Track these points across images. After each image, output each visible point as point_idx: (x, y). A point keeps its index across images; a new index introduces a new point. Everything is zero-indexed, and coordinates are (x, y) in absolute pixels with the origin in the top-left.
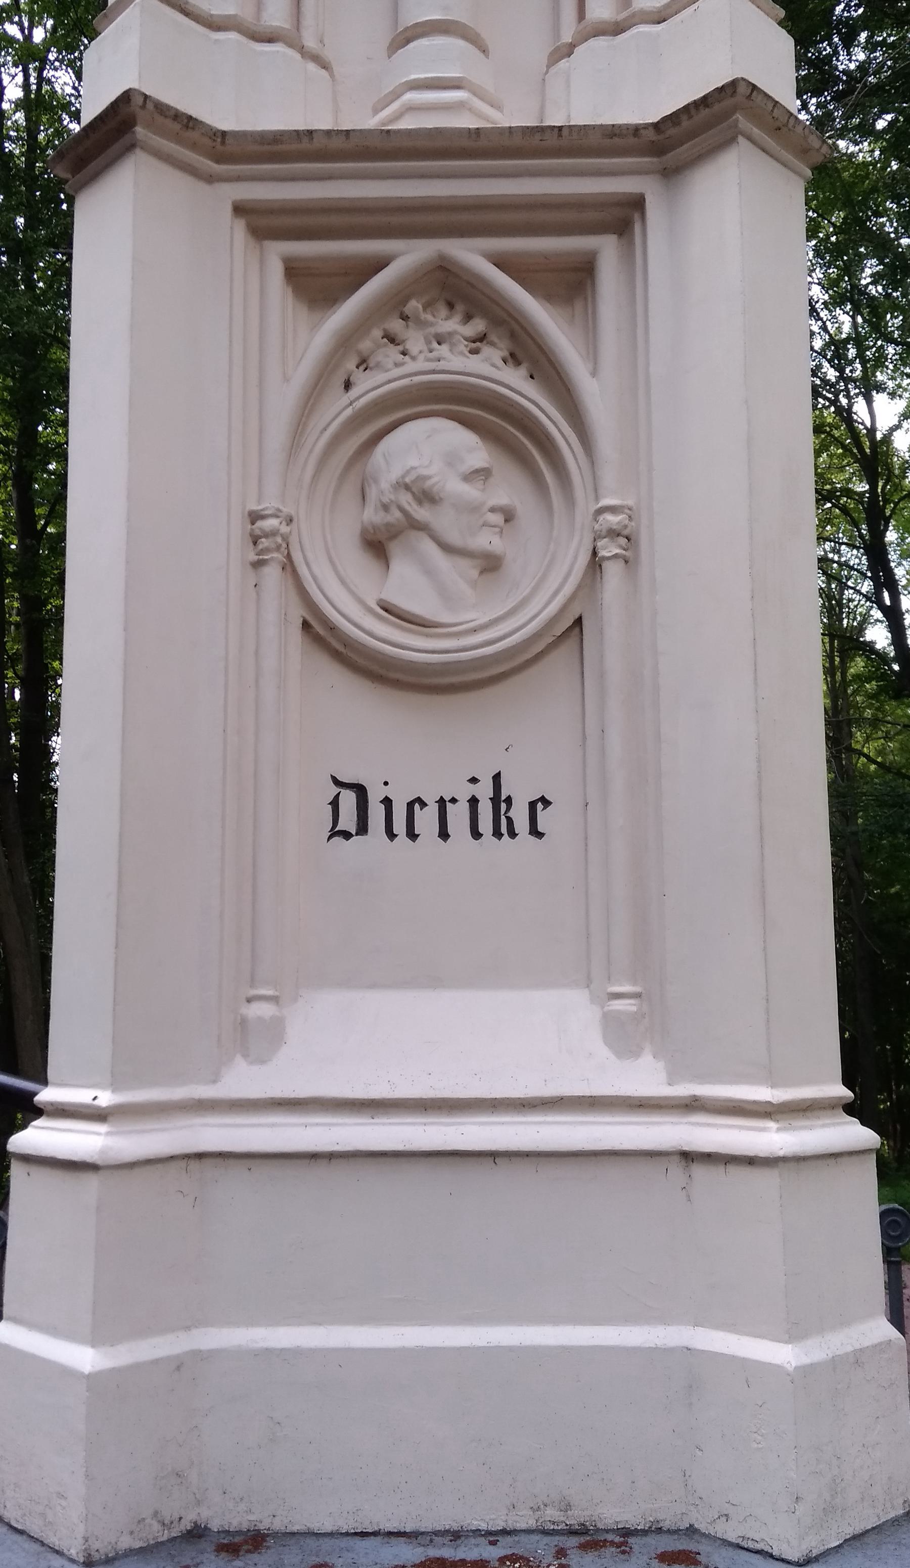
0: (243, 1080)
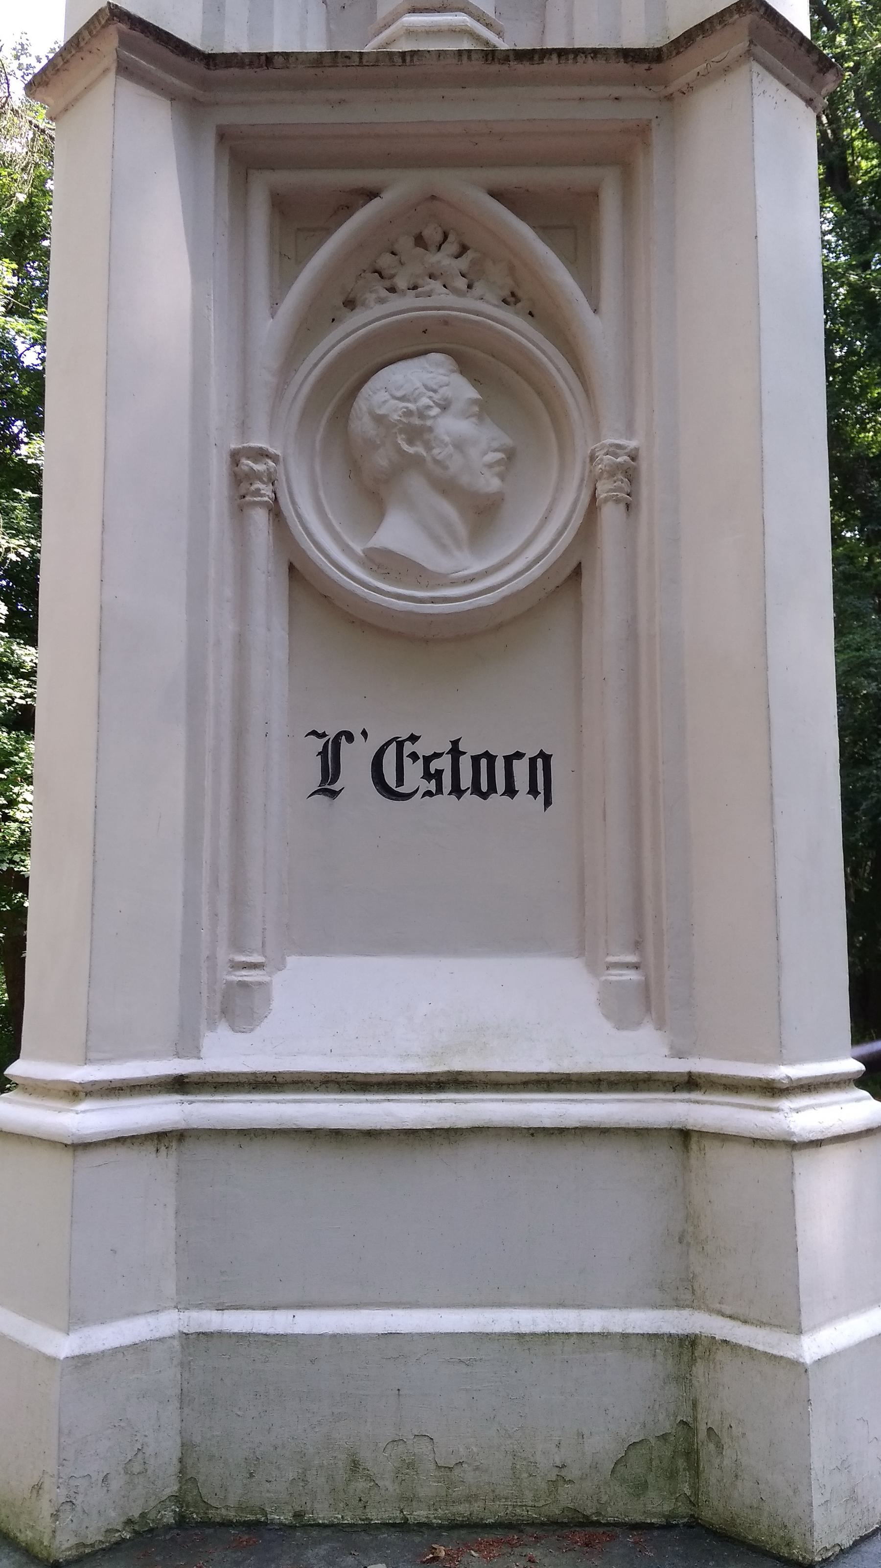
0: (224, 1051)
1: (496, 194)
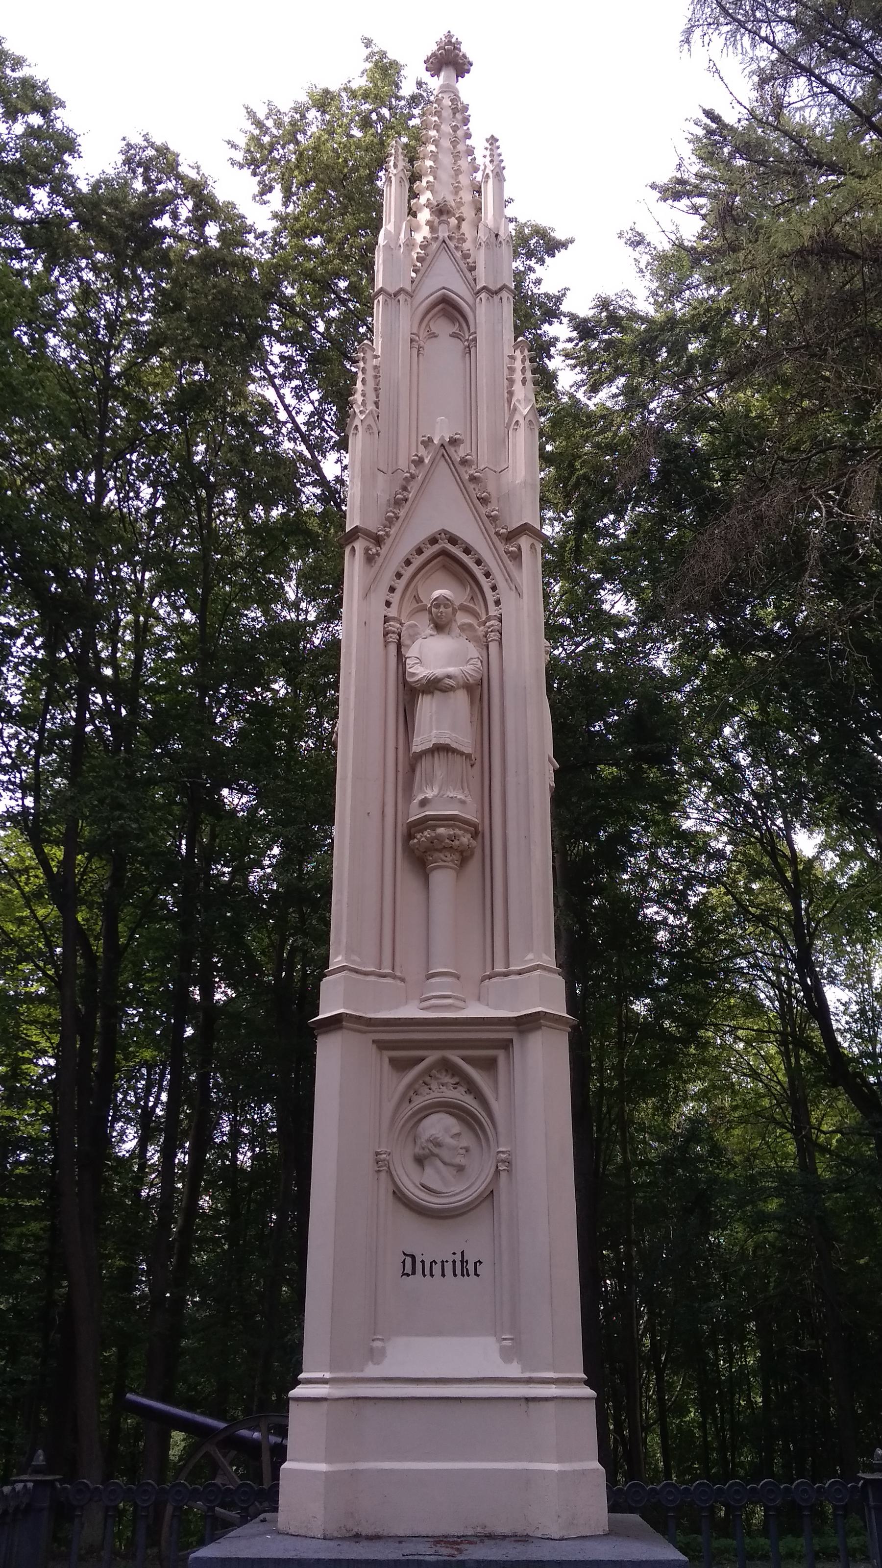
0: (372, 1370)
1: (464, 1059)
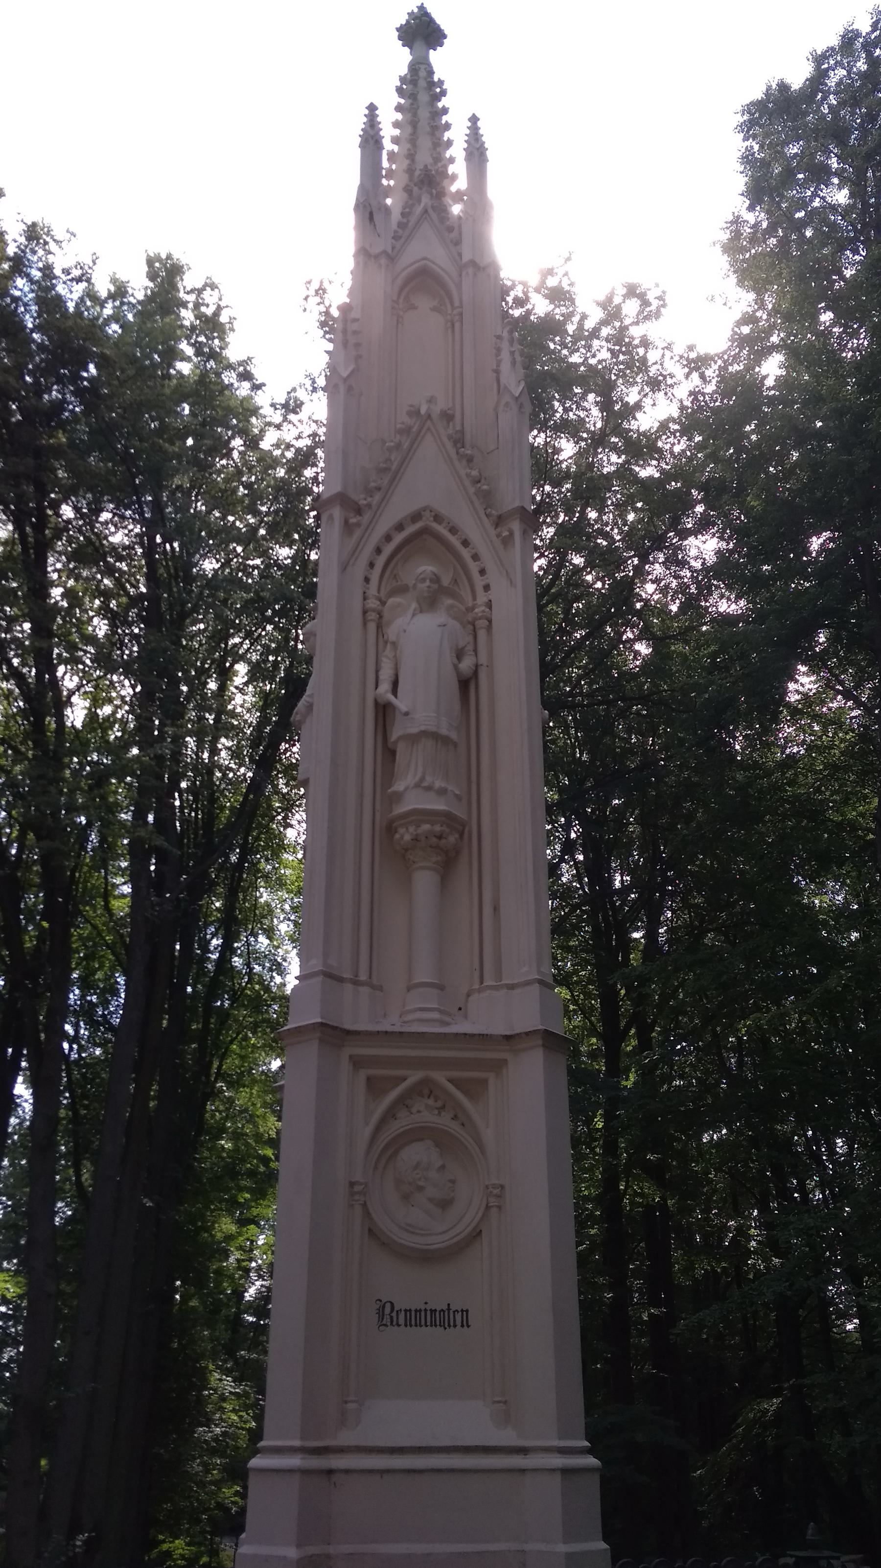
0: (346, 1438)
